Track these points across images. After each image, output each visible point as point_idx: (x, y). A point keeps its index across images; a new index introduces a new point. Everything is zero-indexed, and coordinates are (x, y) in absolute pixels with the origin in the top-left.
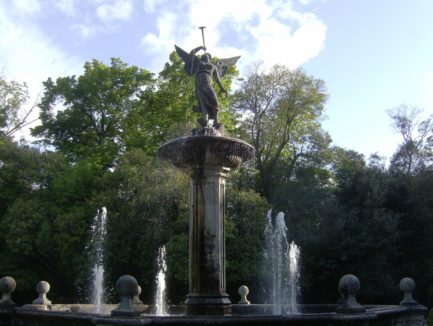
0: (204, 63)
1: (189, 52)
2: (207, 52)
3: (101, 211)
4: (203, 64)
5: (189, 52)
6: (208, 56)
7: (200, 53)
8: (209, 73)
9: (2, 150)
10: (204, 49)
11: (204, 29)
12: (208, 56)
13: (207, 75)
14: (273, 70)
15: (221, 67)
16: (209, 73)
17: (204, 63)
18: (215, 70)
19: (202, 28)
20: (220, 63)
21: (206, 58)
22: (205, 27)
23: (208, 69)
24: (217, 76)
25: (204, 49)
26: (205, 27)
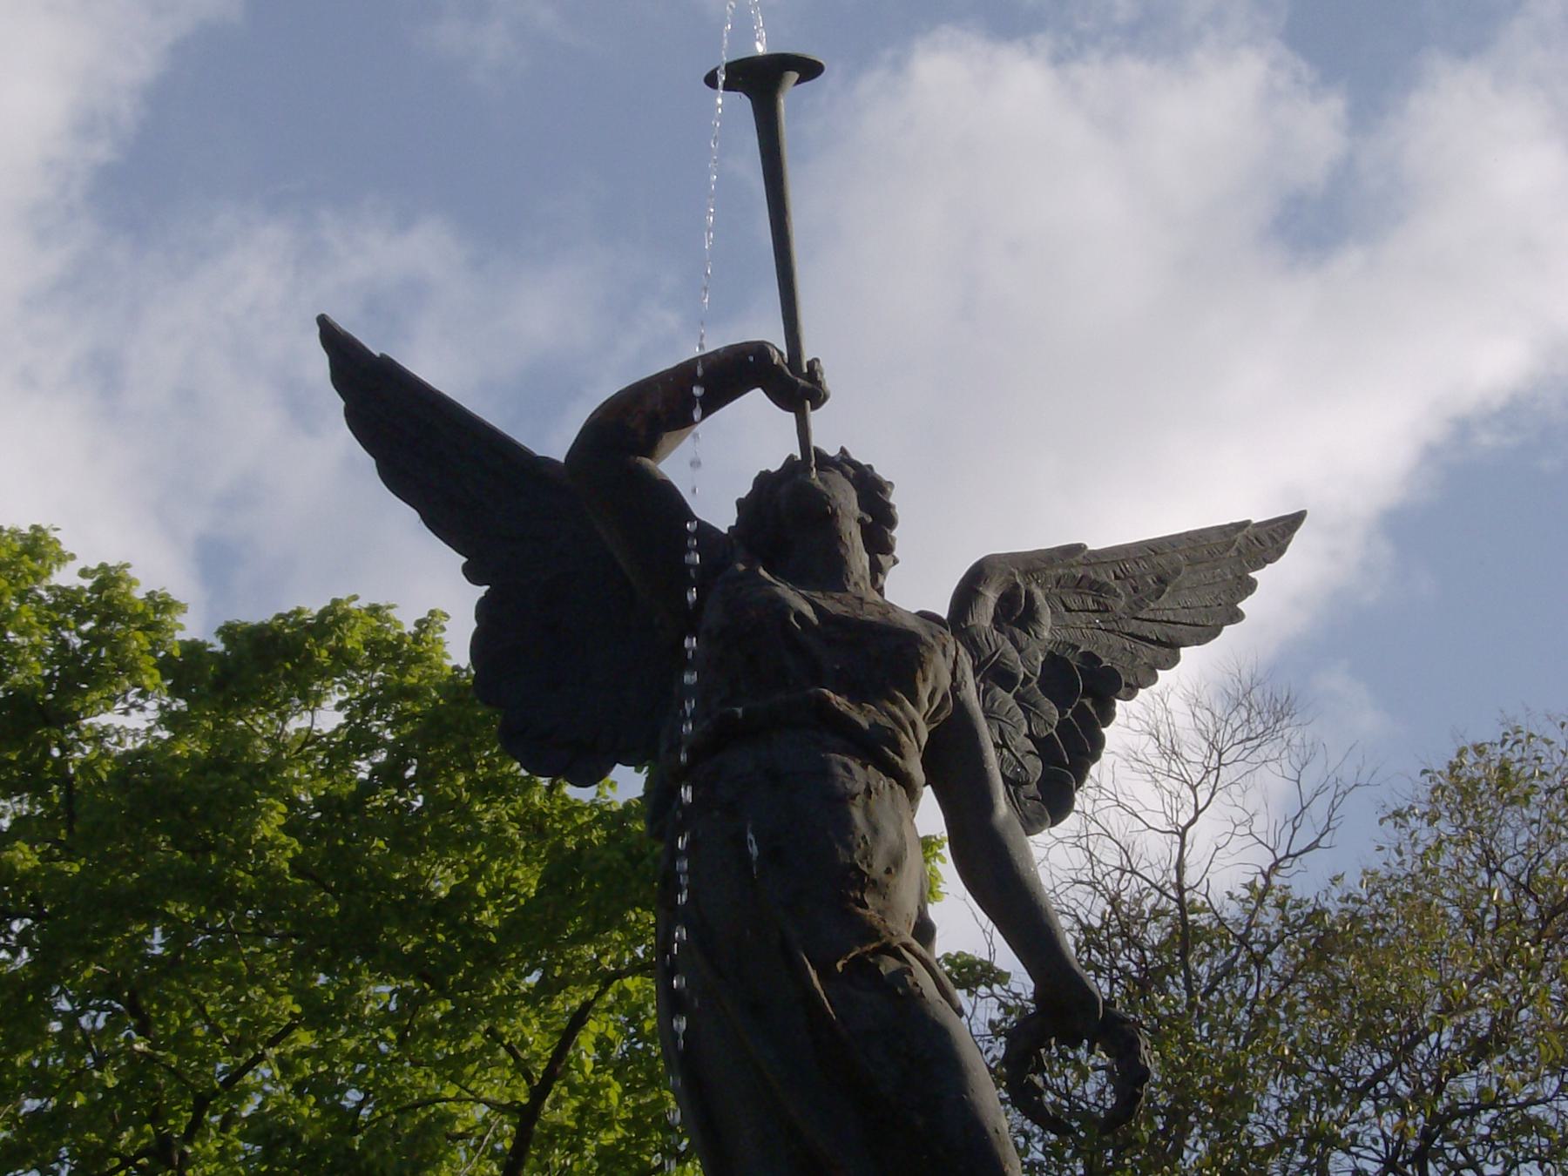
0: (797, 601)
1: (553, 439)
2: (831, 430)
3: (529, 973)
4: (782, 607)
5: (553, 439)
6: (847, 501)
7: (720, 464)
8: (877, 749)
9: (1389, 1163)
10: (797, 388)
11: (791, 97)
12: (847, 501)
13: (861, 775)
14: (1426, 835)
15: (1027, 660)
16: (877, 749)
17: (797, 601)
18: (961, 707)
19: (759, 79)
20: (1008, 602)
21: (822, 517)
22: (809, 69)
23: (858, 696)
24: (988, 805)
25: (797, 388)
26: (809, 69)
